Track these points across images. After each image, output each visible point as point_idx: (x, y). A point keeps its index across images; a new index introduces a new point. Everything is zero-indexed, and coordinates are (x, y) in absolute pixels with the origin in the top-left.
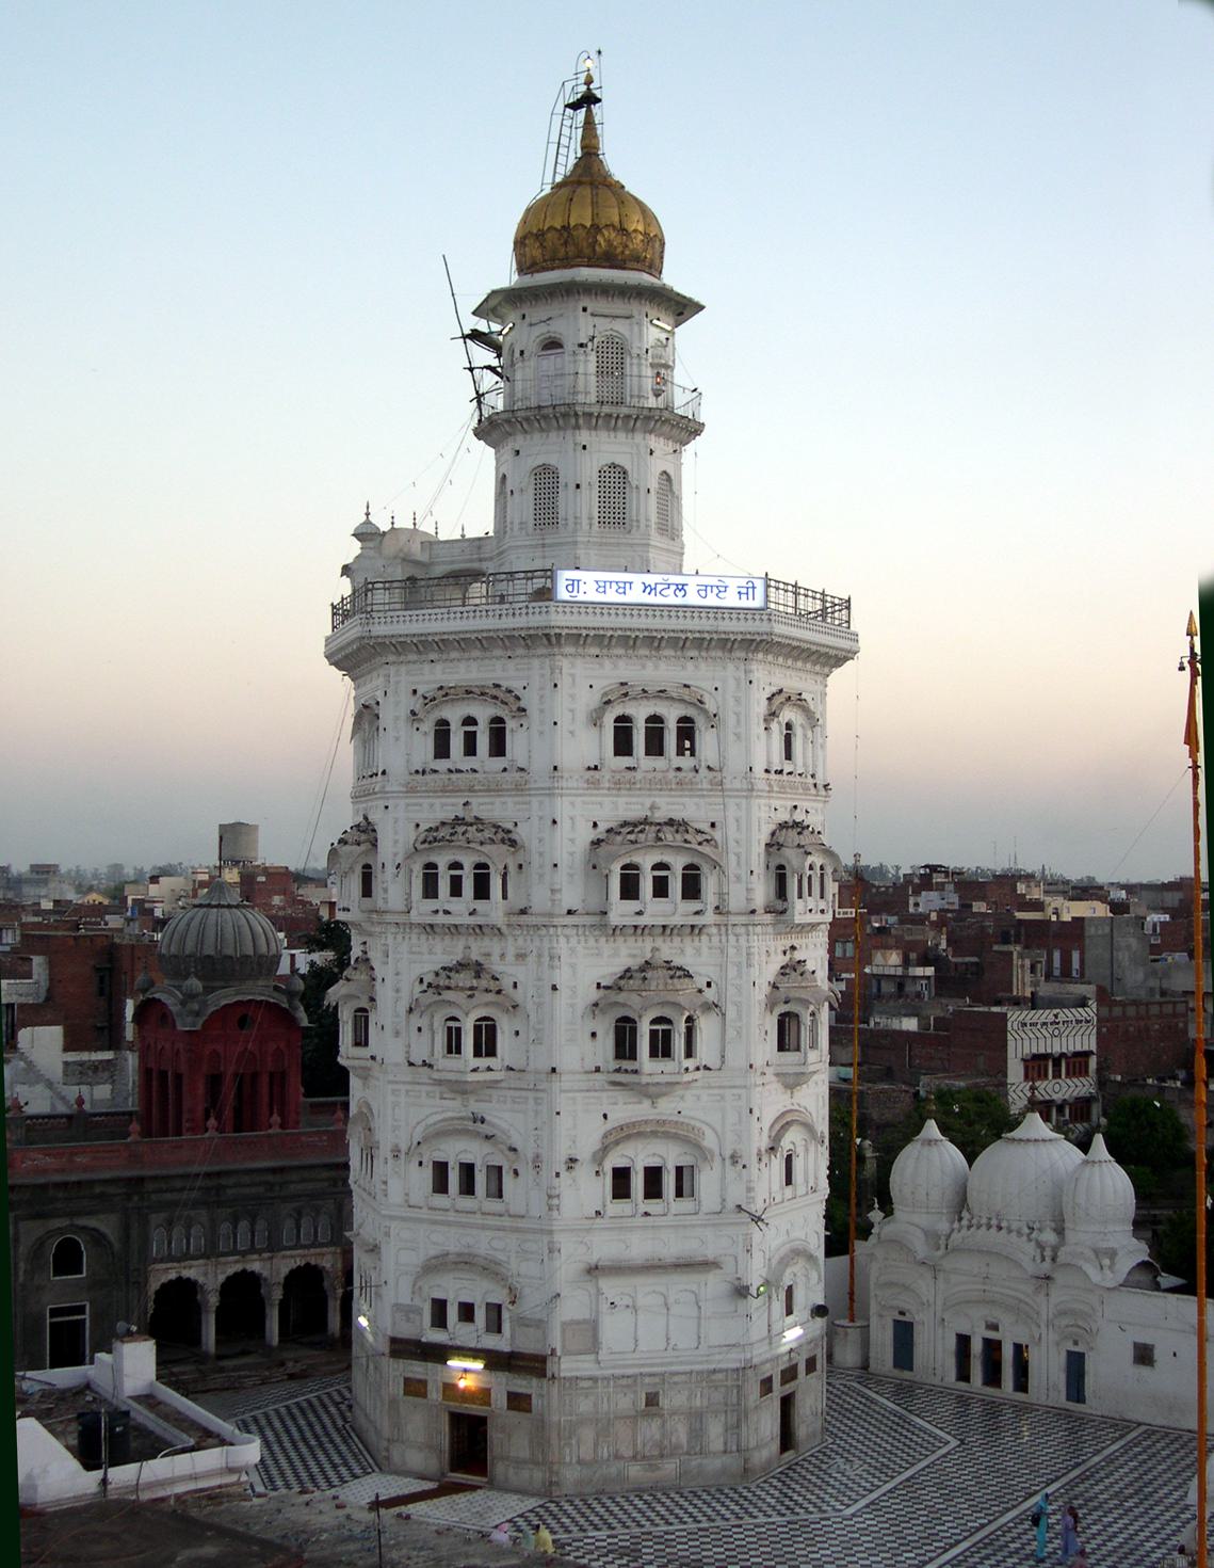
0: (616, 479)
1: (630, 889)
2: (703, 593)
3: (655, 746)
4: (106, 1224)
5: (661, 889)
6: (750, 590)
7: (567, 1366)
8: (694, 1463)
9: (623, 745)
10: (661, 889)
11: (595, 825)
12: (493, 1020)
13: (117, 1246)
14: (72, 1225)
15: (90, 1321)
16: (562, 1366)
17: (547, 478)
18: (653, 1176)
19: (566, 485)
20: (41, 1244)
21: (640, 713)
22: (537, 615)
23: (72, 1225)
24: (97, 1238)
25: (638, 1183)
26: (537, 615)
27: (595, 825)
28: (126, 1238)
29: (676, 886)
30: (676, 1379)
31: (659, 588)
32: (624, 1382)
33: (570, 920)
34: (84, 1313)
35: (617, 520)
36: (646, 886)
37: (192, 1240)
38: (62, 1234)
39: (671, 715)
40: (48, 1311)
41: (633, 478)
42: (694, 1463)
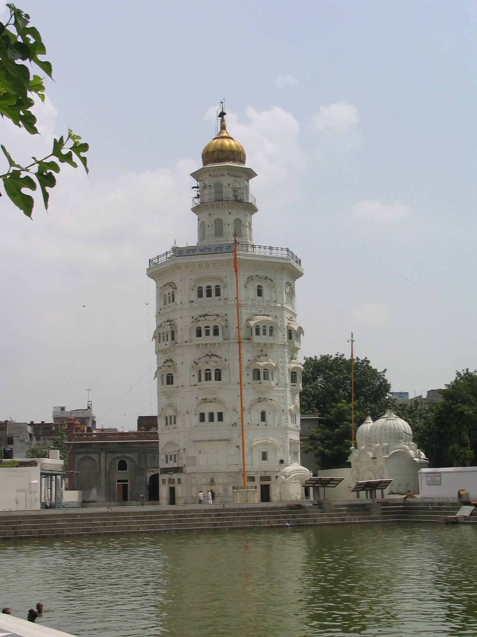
0: (238, 222)
1: (199, 334)
2: (216, 250)
3: (209, 294)
4: (134, 456)
5: (207, 333)
6: (230, 248)
7: (188, 469)
8: (225, 499)
9: (200, 295)
10: (207, 333)
11: (193, 317)
12: (172, 374)
13: (137, 463)
14: (123, 456)
15: (130, 485)
16: (187, 469)
17: (219, 223)
18: (211, 415)
19: (225, 224)
20: (114, 460)
21: (204, 286)
22: (180, 260)
23: (123, 456)
24: (132, 460)
25: (207, 417)
26: (185, 260)
27: (193, 317)
28: (140, 460)
29: (211, 332)
30: (219, 474)
31: (204, 249)
32: (205, 474)
33: (186, 344)
34: (128, 482)
35: (218, 234)
36: (203, 333)
37: (155, 463)
38: (121, 458)
39: (213, 285)
40: (116, 481)
41: (243, 223)
42: (225, 499)
